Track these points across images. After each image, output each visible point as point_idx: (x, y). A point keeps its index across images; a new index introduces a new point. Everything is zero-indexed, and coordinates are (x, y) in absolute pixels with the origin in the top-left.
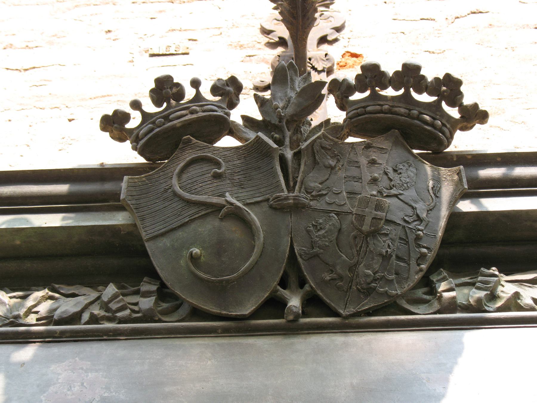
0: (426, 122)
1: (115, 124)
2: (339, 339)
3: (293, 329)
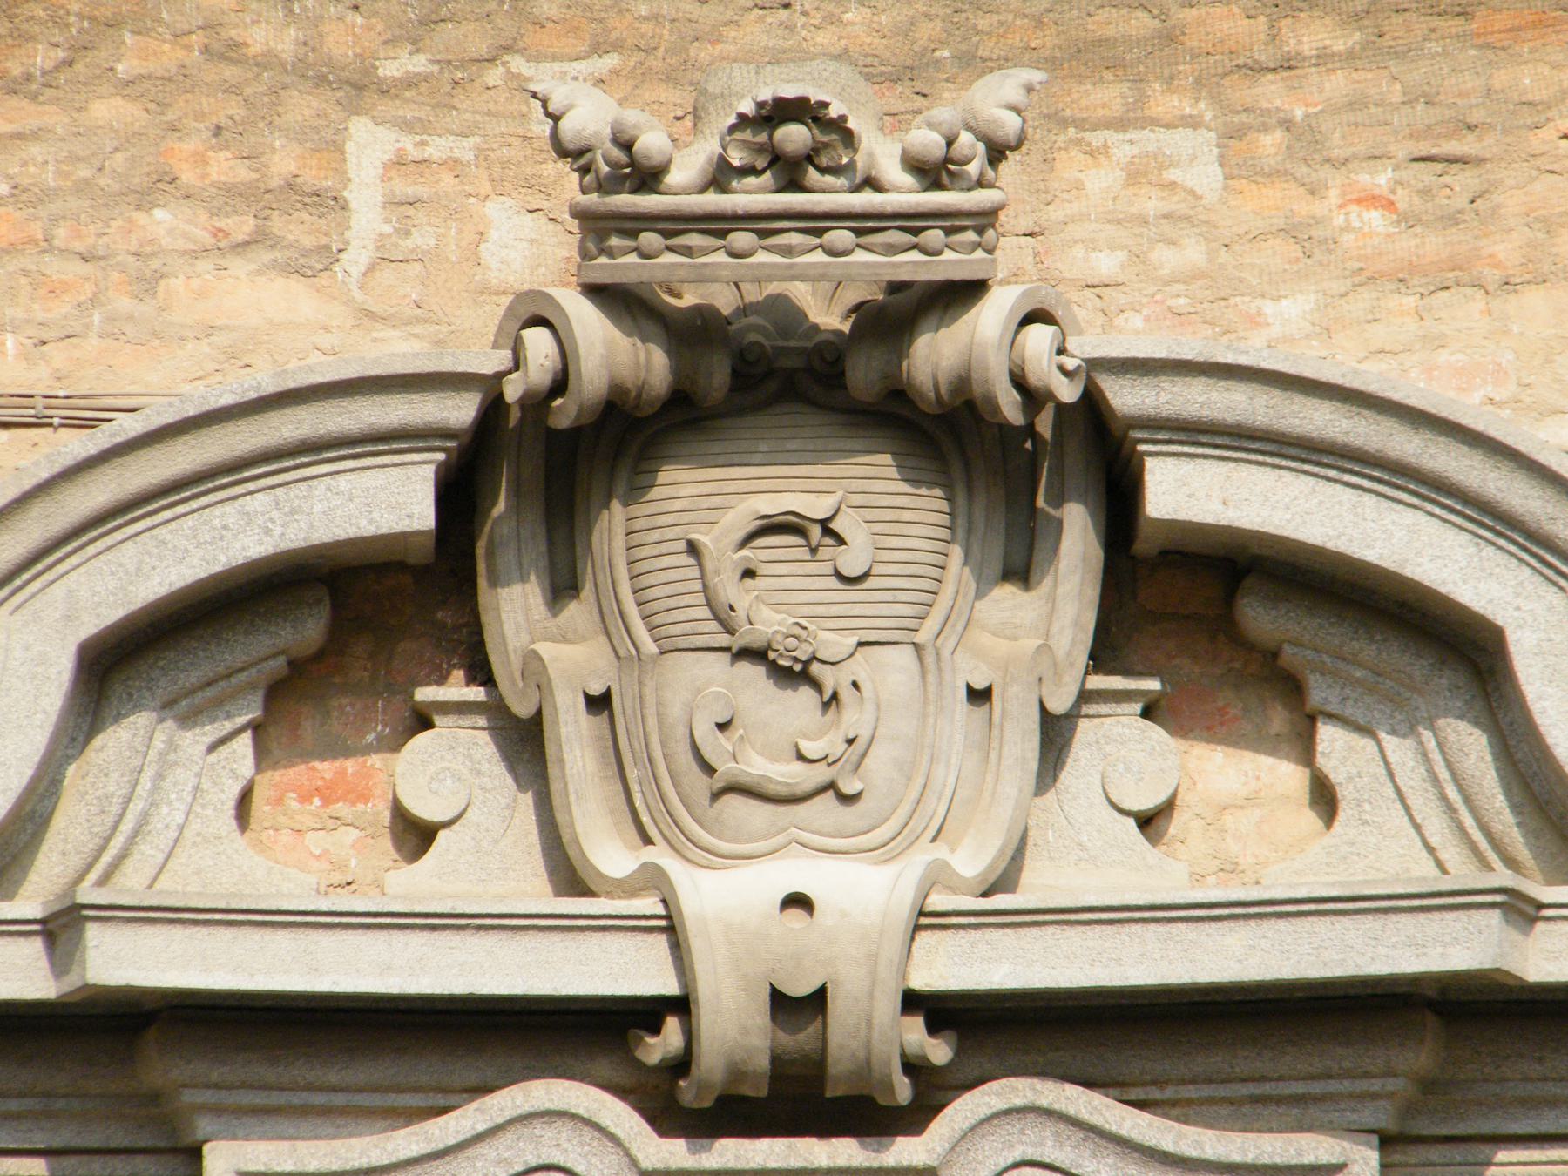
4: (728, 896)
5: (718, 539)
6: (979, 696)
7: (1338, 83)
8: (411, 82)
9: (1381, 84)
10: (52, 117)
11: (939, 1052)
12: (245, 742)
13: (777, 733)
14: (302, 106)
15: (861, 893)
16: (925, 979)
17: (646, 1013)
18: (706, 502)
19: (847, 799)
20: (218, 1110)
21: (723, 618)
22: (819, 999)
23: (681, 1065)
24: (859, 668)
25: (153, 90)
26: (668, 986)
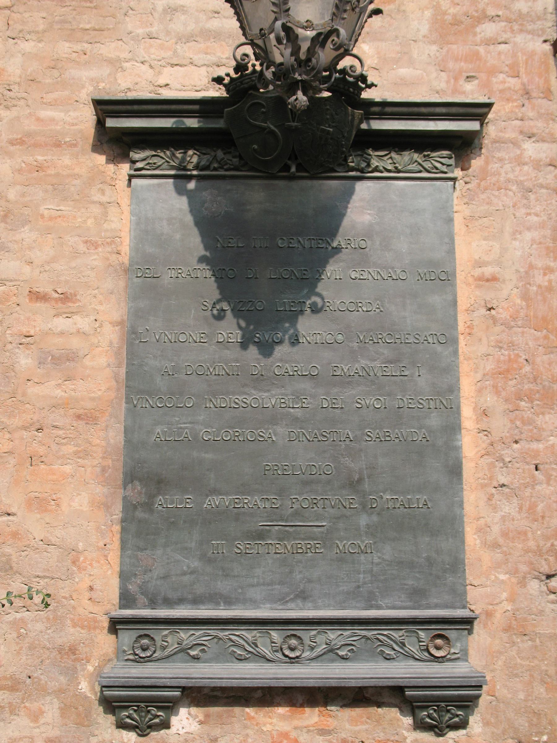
0: (350, 92)
1: (218, 80)
2: (309, 183)
3: (292, 178)
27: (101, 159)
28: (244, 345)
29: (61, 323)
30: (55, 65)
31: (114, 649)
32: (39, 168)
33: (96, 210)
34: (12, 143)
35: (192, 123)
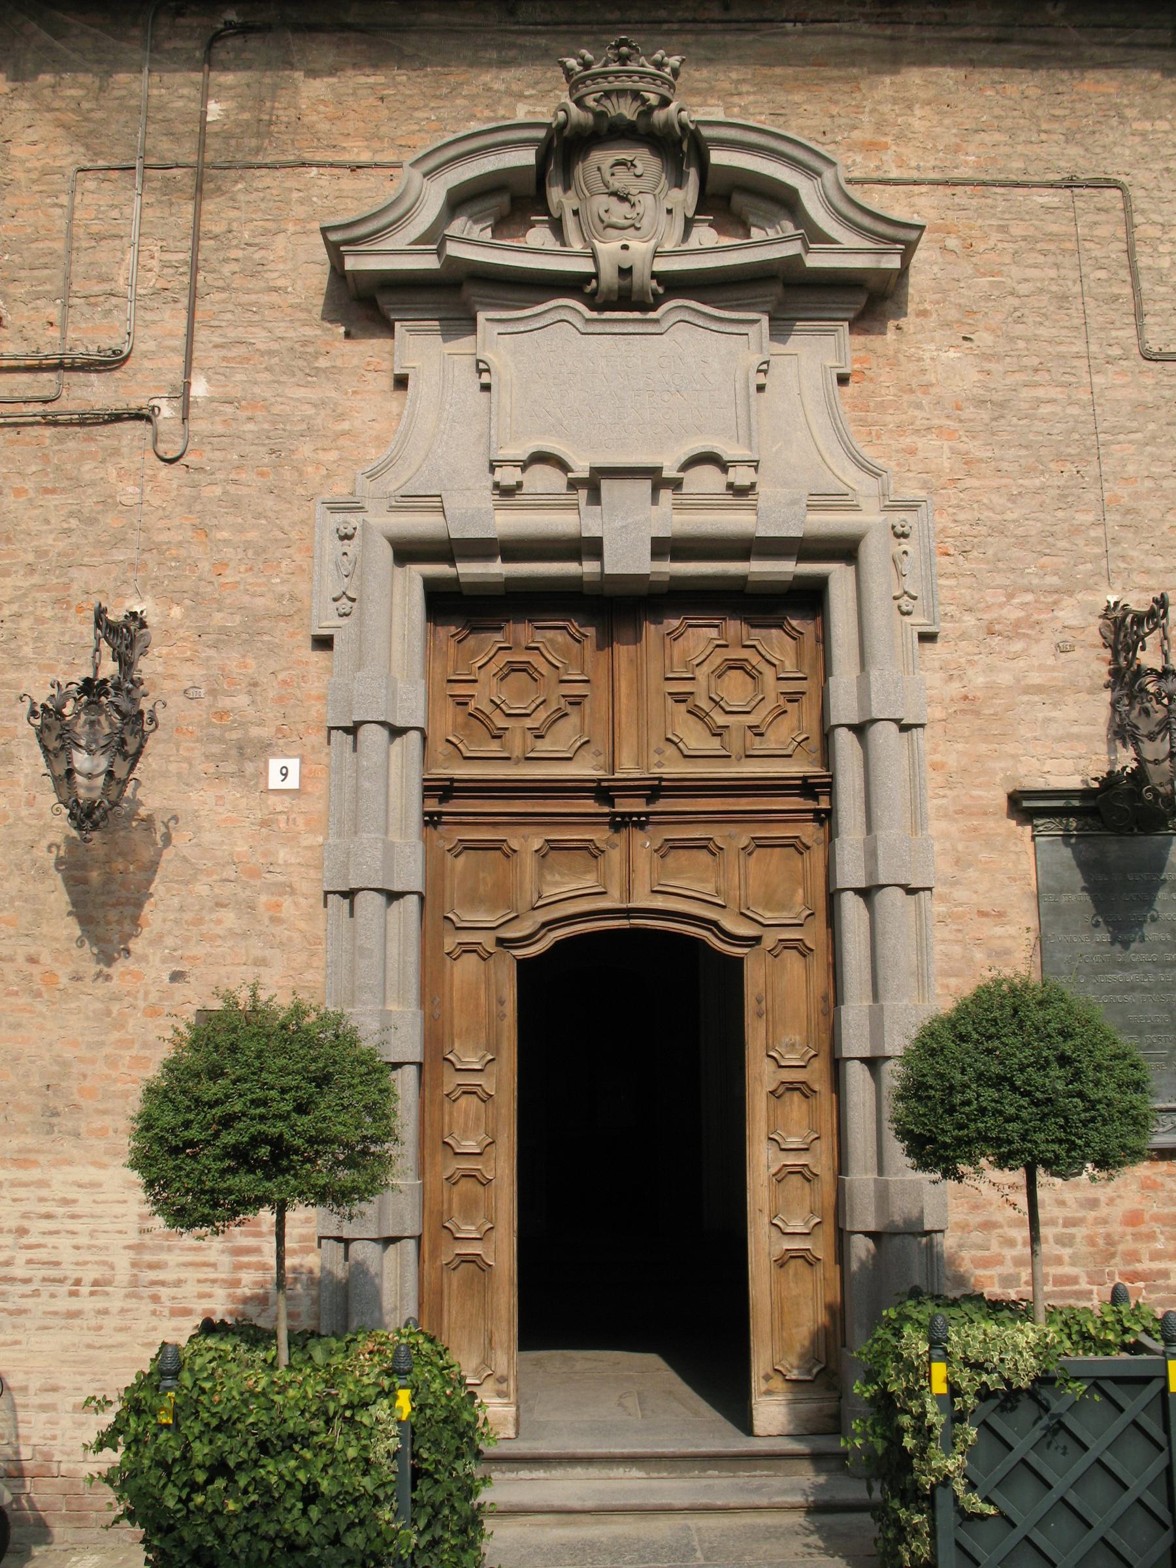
4: (609, 248)
5: (606, 167)
6: (669, 212)
7: (751, 98)
8: (531, 96)
9: (759, 98)
10: (448, 104)
11: (661, 290)
12: (489, 230)
13: (619, 212)
14: (506, 101)
15: (640, 248)
16: (655, 269)
17: (587, 278)
18: (603, 157)
19: (638, 229)
20: (481, 304)
21: (606, 185)
22: (630, 270)
23: (595, 293)
24: (640, 197)
25: (472, 98)
26: (593, 270)
27: (1014, 823)
28: (1112, 943)
29: (999, 931)
30: (978, 759)
31: (284, 1001)
32: (975, 830)
33: (1013, 856)
34: (956, 812)
35: (1076, 803)
